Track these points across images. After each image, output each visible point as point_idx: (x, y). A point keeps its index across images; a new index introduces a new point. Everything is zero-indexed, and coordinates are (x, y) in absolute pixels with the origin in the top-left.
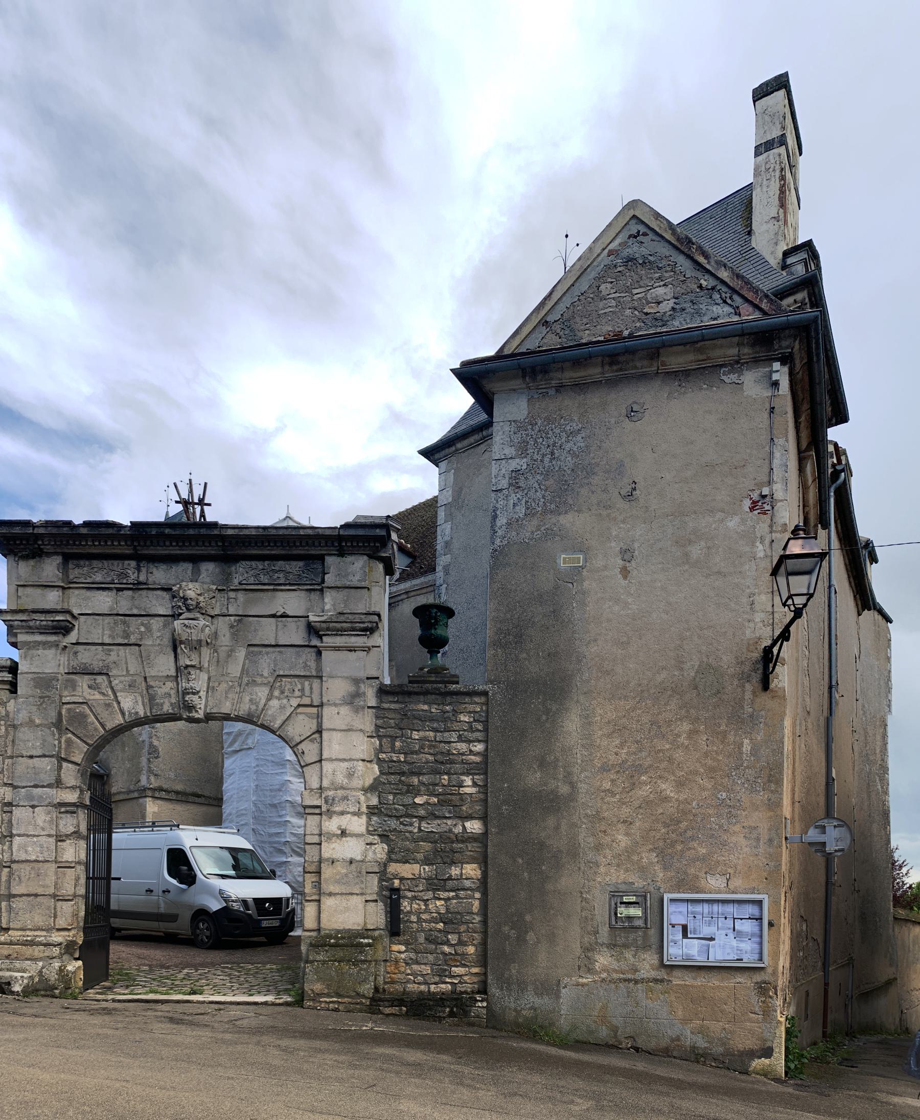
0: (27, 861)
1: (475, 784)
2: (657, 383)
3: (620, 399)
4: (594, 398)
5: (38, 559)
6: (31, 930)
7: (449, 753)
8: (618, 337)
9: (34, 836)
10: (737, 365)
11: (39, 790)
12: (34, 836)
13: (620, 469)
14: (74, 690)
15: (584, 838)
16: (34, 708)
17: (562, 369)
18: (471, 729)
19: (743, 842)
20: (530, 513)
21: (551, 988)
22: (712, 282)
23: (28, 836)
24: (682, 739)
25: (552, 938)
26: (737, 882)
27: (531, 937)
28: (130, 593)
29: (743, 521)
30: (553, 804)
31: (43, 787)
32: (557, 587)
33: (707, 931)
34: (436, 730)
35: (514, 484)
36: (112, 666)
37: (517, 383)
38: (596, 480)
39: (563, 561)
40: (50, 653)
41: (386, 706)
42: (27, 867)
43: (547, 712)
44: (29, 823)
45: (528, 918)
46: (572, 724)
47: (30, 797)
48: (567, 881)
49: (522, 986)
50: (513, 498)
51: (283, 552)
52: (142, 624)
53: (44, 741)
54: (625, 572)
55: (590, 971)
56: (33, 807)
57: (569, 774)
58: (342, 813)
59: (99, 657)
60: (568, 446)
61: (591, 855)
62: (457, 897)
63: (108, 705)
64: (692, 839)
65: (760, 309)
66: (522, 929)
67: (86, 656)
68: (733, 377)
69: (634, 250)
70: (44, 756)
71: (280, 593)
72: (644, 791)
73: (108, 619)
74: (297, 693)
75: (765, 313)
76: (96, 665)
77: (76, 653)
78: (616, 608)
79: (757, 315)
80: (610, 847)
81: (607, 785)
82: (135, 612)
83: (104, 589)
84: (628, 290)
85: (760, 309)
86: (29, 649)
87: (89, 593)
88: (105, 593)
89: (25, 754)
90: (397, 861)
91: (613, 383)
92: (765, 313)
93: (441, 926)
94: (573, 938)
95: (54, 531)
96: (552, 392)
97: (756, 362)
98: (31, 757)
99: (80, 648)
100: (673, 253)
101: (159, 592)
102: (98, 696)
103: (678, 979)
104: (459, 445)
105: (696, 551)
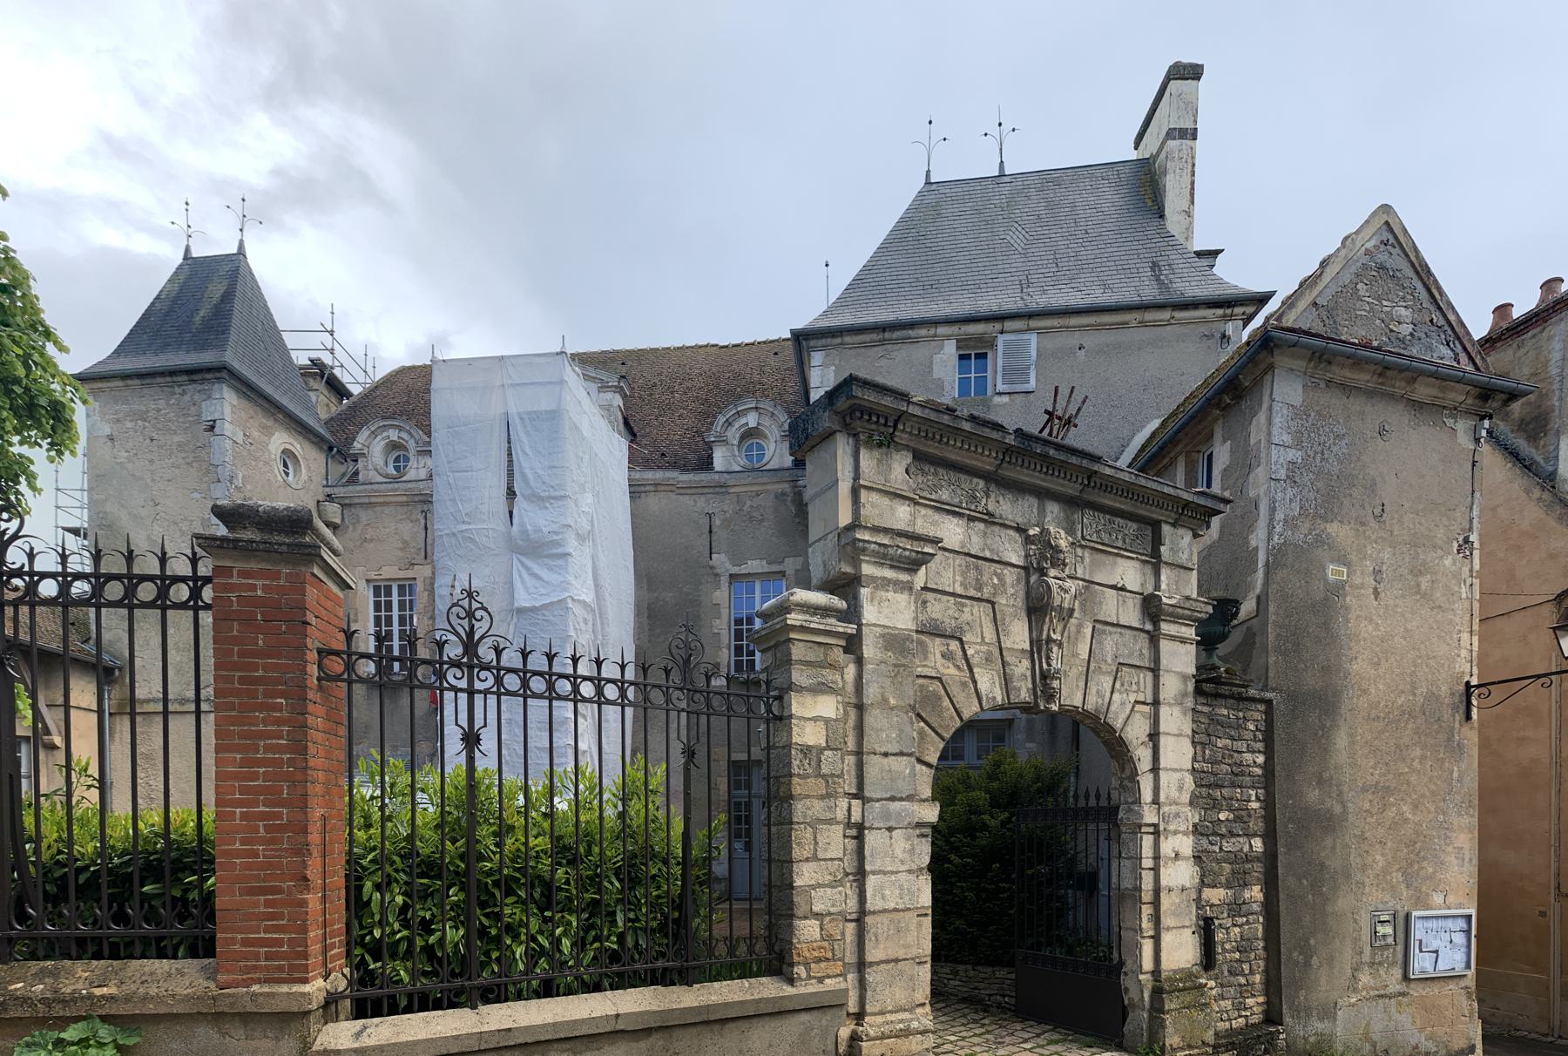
0: (885, 911)
1: (1258, 799)
2: (1401, 407)
3: (1377, 413)
4: (1356, 404)
5: (884, 450)
6: (891, 1012)
7: (1241, 764)
8: (1366, 346)
9: (892, 872)
10: (1455, 411)
11: (897, 804)
12: (892, 872)
13: (1372, 488)
14: (926, 658)
15: (1355, 860)
16: (888, 682)
17: (1343, 366)
18: (1255, 739)
19: (1455, 862)
20: (1303, 512)
21: (1329, 1012)
22: (1442, 322)
23: (885, 873)
24: (1416, 764)
25: (1330, 961)
26: (1451, 899)
27: (1315, 961)
28: (981, 526)
29: (1454, 561)
30: (1329, 823)
31: (901, 799)
32: (1326, 599)
33: (1434, 945)
34: (1233, 739)
35: (1291, 479)
36: (966, 628)
37: (1300, 364)
38: (1356, 492)
39: (1334, 572)
40: (902, 599)
41: (1199, 708)
42: (884, 919)
43: (1323, 727)
44: (886, 855)
45: (1312, 942)
46: (1341, 740)
47: (886, 815)
48: (1343, 903)
49: (1308, 1012)
50: (1290, 493)
51: (1131, 509)
52: (996, 574)
53: (901, 731)
54: (1376, 593)
55: (1355, 990)
56: (890, 829)
57: (1340, 794)
58: (1176, 833)
59: (950, 612)
60: (1335, 449)
61: (1359, 877)
62: (1248, 922)
63: (964, 684)
64: (1424, 858)
65: (1475, 364)
66: (1308, 953)
67: (939, 609)
68: (1450, 422)
69: (1382, 257)
70: (901, 754)
71: (1120, 560)
72: (1391, 813)
73: (959, 560)
74: (1134, 687)
75: (1478, 369)
76: (949, 625)
77: (924, 602)
78: (1370, 628)
79: (1470, 368)
80: (1371, 867)
81: (1367, 806)
82: (988, 554)
83: (949, 512)
84: (1379, 299)
85: (1475, 364)
86: (876, 588)
87: (937, 516)
88: (955, 520)
89: (878, 750)
90: (1209, 886)
91: (1371, 394)
92: (1478, 369)
93: (1237, 955)
94: (1346, 959)
95: (933, 416)
96: (1323, 385)
97: (1468, 413)
98: (886, 755)
99: (930, 596)
100: (1411, 274)
101: (1011, 532)
102: (953, 671)
103: (1416, 991)
104: (847, 339)
105: (1425, 582)
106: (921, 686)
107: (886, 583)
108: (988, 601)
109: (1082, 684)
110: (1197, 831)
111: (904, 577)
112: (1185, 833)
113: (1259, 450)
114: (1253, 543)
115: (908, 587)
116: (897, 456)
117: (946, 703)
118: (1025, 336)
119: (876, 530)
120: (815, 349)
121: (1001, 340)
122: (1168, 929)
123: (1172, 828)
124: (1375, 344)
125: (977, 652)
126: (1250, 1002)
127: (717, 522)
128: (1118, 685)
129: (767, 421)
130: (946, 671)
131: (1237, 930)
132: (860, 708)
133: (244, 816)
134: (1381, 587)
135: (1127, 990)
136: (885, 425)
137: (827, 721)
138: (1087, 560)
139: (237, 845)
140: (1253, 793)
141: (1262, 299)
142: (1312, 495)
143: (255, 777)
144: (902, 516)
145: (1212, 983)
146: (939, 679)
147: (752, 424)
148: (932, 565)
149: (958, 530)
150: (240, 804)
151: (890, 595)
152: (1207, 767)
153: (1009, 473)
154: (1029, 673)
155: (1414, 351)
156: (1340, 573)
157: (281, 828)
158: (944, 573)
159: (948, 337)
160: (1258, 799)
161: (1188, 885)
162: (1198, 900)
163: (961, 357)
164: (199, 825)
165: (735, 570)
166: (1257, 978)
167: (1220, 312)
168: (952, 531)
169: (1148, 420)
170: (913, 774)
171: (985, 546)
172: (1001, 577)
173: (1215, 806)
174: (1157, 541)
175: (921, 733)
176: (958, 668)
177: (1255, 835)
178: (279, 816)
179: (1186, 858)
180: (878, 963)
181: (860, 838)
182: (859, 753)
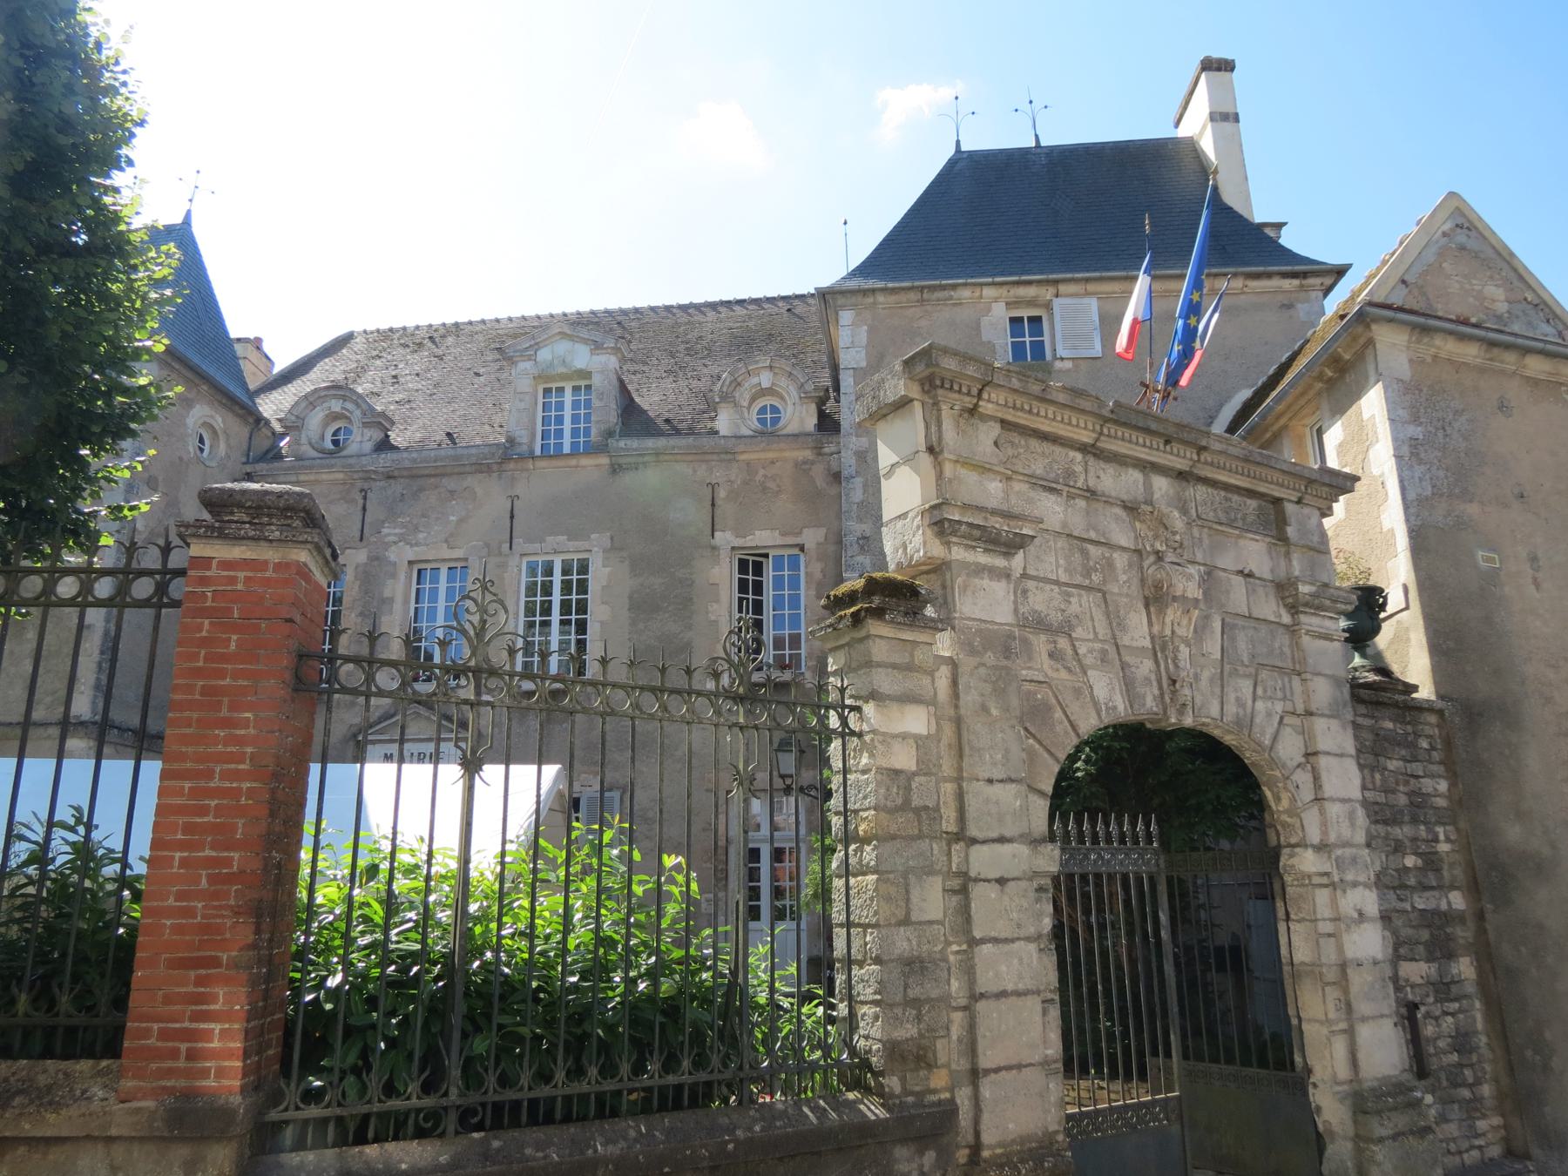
14: (1030, 659)
36: (1074, 622)
40: (1000, 588)
41: (1360, 720)
58: (1355, 884)
59: (1055, 603)
63: (1077, 692)
67: (1041, 600)
70: (1011, 780)
76: (1055, 618)
77: (1025, 592)
78: (1538, 623)
82: (1093, 535)
88: (1053, 498)
90: (1406, 959)
93: (1455, 1057)
98: (990, 781)
99: (1031, 584)
102: (1063, 674)
106: (1029, 692)
107: (980, 570)
108: (1099, 590)
109: (1218, 690)
110: (1381, 883)
111: (999, 562)
112: (1366, 886)
113: (1374, 425)
114: (1387, 525)
115: (1007, 575)
116: (983, 427)
117: (1058, 714)
118: (1086, 300)
119: (966, 507)
120: (843, 307)
121: (1057, 303)
122: (1364, 1019)
123: (1349, 877)
124: (1473, 320)
125: (1091, 651)
126: (1482, 1125)
127: (722, 493)
128: (1260, 691)
129: (783, 382)
130: (1055, 675)
131: (1450, 1019)
132: (958, 722)
133: (184, 863)
134: (1540, 575)
135: (1319, 1109)
136: (969, 394)
137: (917, 738)
138: (1206, 541)
139: (171, 902)
140: (1440, 830)
141: (1340, 272)
142: (1441, 473)
143: (203, 811)
144: (992, 491)
145: (1429, 1099)
146: (1050, 687)
147: (765, 384)
148: (1031, 548)
149: (1058, 509)
150: (182, 846)
151: (986, 582)
152: (1381, 798)
153: (1106, 444)
154: (1153, 677)
155: (1516, 328)
156: (1491, 560)
157: (230, 879)
158: (1050, 561)
159: (996, 300)
160: (1448, 840)
161: (1380, 956)
162: (1395, 979)
163: (1013, 320)
164: (465, 860)
165: (738, 542)
166: (1486, 1090)
167: (1296, 282)
168: (1052, 510)
169: (1236, 390)
170: (1026, 808)
171: (1090, 526)
172: (1110, 564)
173: (1398, 848)
174: (1281, 521)
175: (1031, 754)
176: (1069, 670)
177: (1453, 887)
178: (228, 862)
179: (1372, 920)
180: (997, 1070)
181: (964, 891)
182: (959, 779)
